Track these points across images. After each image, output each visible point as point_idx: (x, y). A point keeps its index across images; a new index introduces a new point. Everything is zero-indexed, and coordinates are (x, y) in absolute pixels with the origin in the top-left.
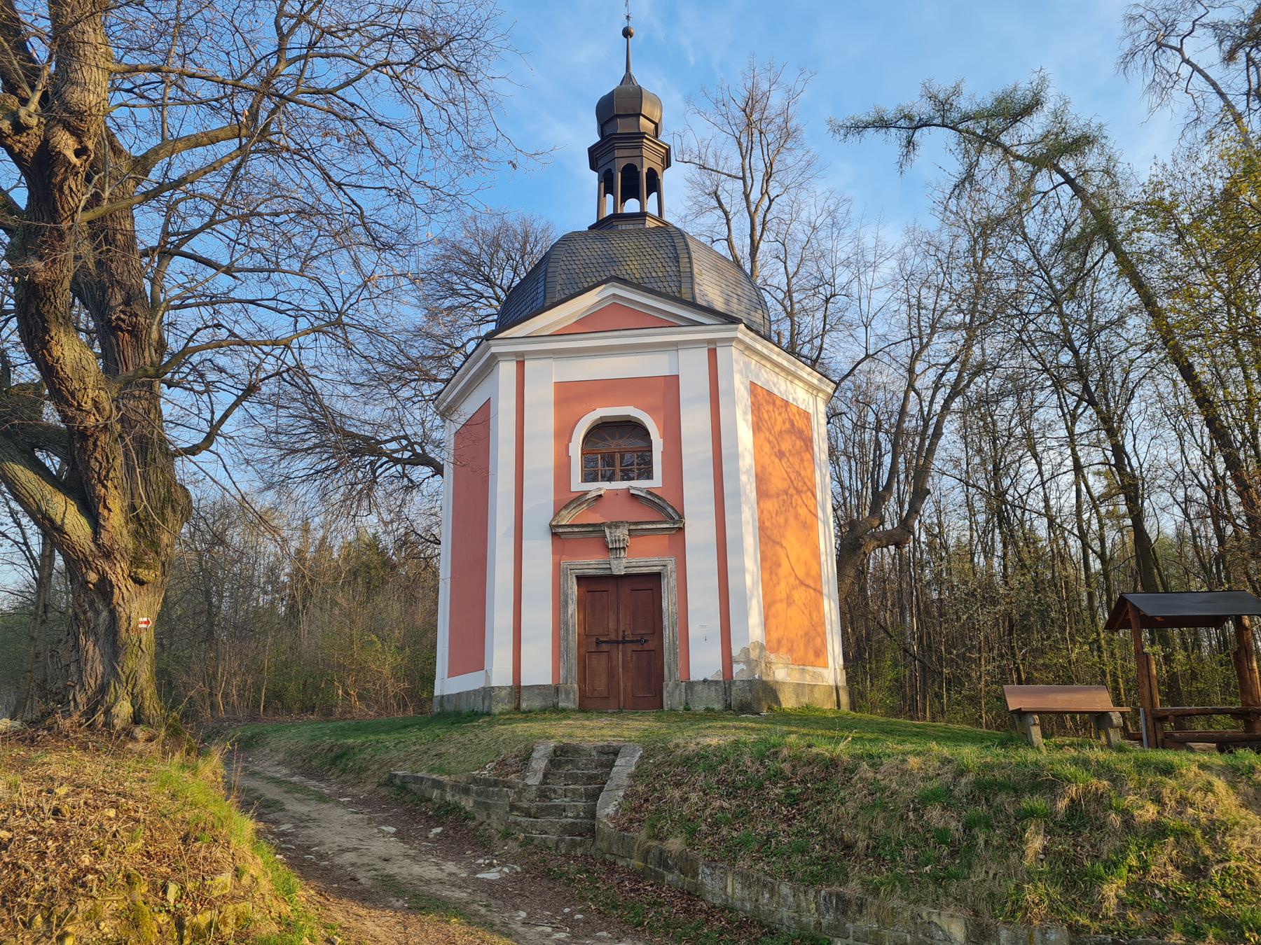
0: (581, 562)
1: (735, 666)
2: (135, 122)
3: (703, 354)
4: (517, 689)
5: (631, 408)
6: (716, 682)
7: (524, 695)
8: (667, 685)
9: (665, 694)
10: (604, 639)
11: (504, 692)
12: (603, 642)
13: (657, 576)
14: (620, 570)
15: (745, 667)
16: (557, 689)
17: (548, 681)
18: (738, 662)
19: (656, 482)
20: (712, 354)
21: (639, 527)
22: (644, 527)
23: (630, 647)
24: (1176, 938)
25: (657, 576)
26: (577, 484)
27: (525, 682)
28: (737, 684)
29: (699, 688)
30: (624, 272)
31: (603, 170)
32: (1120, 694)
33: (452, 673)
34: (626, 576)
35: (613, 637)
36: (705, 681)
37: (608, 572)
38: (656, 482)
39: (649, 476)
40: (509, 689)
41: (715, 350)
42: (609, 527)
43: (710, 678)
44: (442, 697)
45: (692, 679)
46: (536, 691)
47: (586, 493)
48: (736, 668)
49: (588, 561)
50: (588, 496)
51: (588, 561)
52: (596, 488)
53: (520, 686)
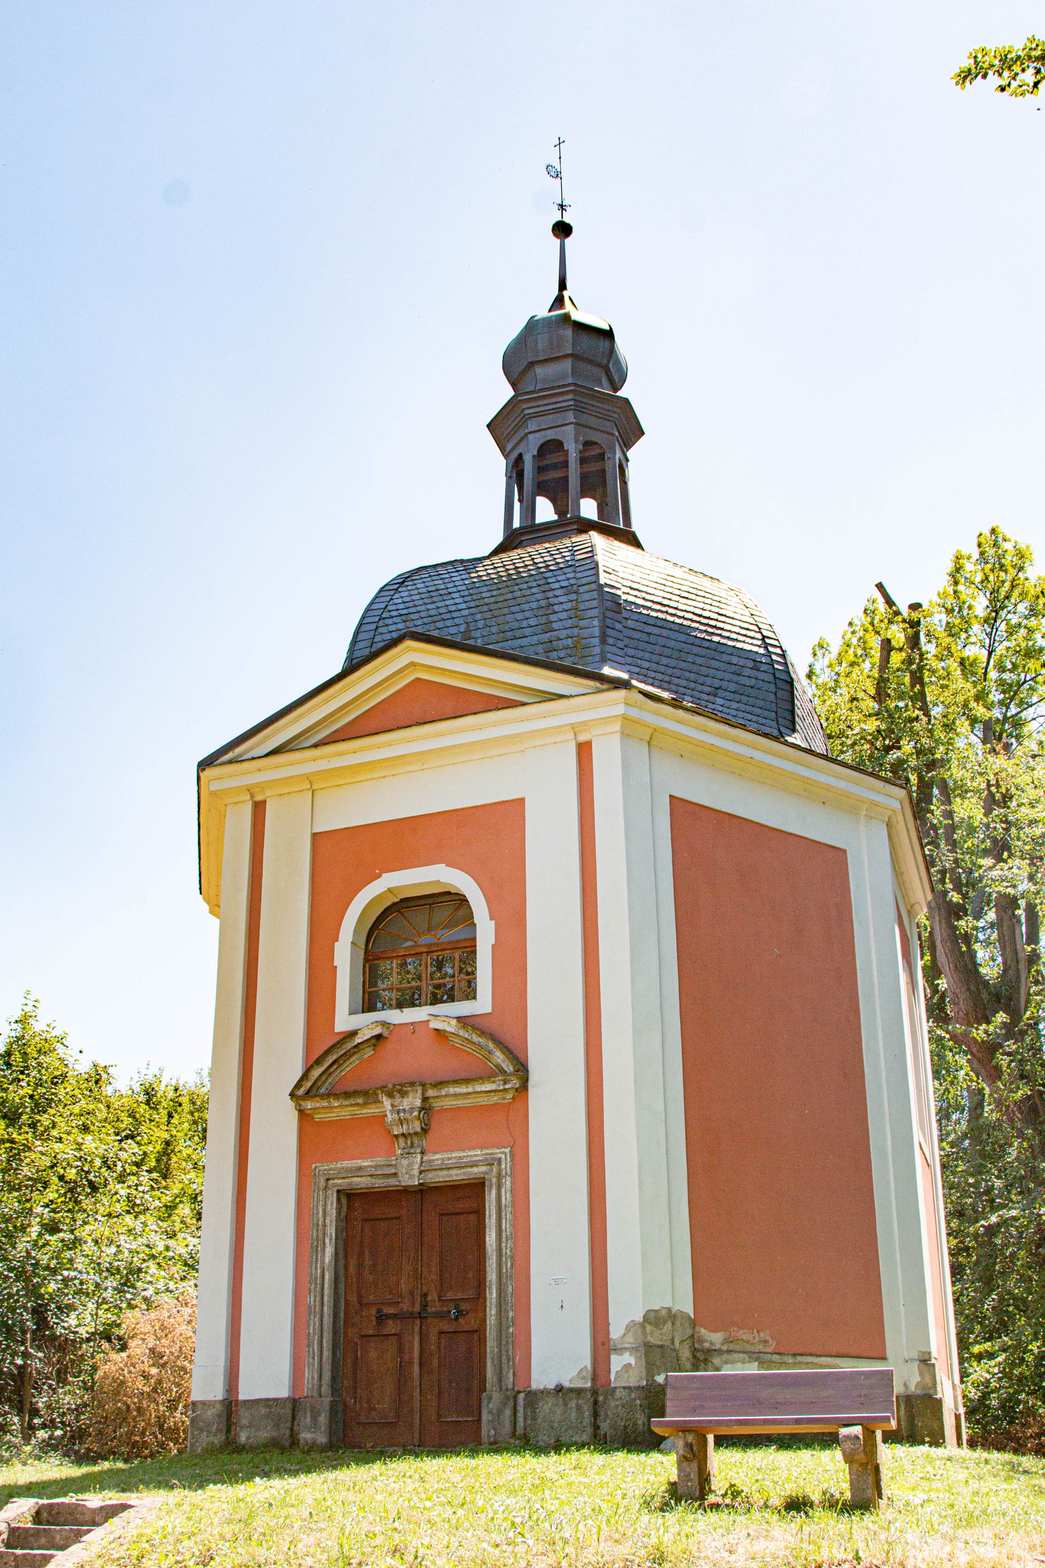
0: (347, 1164)
1: (614, 1358)
4: (230, 1406)
6: (579, 1392)
7: (244, 1417)
8: (490, 1398)
9: (485, 1417)
10: (391, 1310)
11: (210, 1413)
12: (388, 1316)
13: (477, 1188)
14: (411, 1177)
15: (632, 1360)
16: (294, 1404)
17: (283, 1391)
18: (619, 1351)
19: (483, 1003)
22: (452, 1090)
23: (435, 1327)
24: (341, 1565)
25: (477, 1188)
26: (344, 1020)
27: (245, 1394)
28: (618, 1394)
29: (546, 1407)
31: (514, 456)
35: (405, 1306)
36: (559, 1389)
37: (392, 1181)
38: (483, 1003)
39: (471, 994)
40: (219, 1406)
42: (390, 1095)
43: (566, 1384)
45: (534, 1386)
46: (263, 1411)
48: (617, 1362)
50: (358, 1040)
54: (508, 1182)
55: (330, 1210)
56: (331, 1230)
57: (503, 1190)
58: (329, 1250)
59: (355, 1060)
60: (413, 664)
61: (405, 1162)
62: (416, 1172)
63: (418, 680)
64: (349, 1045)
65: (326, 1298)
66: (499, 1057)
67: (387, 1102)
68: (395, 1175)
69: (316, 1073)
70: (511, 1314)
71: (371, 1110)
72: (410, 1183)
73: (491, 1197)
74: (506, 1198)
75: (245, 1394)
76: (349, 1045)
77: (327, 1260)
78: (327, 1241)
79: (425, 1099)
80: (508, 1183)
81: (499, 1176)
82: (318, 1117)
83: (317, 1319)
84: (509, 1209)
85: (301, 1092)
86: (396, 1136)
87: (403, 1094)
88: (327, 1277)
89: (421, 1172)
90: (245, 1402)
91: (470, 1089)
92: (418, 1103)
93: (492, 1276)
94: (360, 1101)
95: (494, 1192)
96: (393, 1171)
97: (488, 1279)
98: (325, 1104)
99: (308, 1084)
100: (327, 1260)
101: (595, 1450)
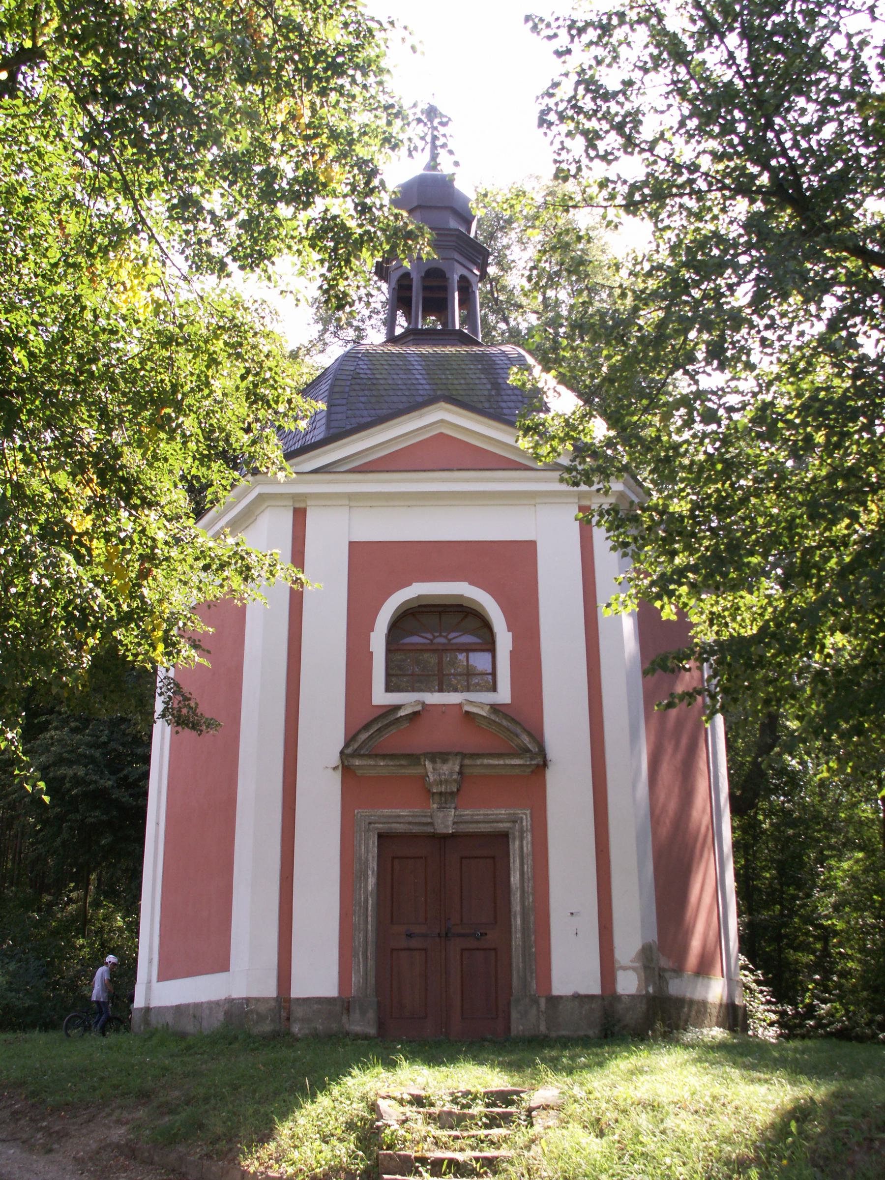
2: (291, 220)
3: (287, 519)
5: (465, 585)
13: (503, 838)
14: (447, 827)
20: (300, 516)
21: (479, 762)
22: (486, 761)
25: (503, 838)
26: (380, 696)
27: (298, 991)
30: (404, 399)
32: (452, 1162)
33: (166, 973)
34: (453, 835)
37: (430, 829)
38: (504, 694)
41: (305, 510)
42: (433, 760)
44: (147, 1010)
45: (555, 992)
47: (398, 708)
49: (398, 811)
50: (402, 713)
51: (398, 811)
52: (407, 700)
53: (288, 1000)
54: (529, 837)
55: (370, 850)
56: (373, 864)
57: (525, 843)
58: (372, 881)
59: (393, 730)
60: (442, 421)
61: (441, 815)
62: (450, 823)
63: (441, 434)
64: (392, 718)
65: (369, 919)
66: (525, 739)
67: (429, 765)
68: (432, 824)
69: (363, 736)
70: (533, 938)
71: (419, 771)
72: (445, 831)
73: (515, 846)
74: (527, 848)
75: (298, 991)
76: (392, 718)
77: (370, 888)
78: (370, 873)
79: (461, 766)
80: (529, 837)
81: (522, 832)
82: (359, 772)
83: (361, 935)
84: (530, 857)
85: (349, 751)
86: (434, 793)
87: (445, 761)
88: (370, 902)
89: (454, 823)
90: (298, 999)
91: (501, 762)
92: (457, 768)
93: (517, 907)
94: (403, 762)
95: (517, 843)
96: (429, 820)
97: (513, 910)
98: (372, 763)
99: (356, 746)
100: (370, 888)
101: (249, 1147)
